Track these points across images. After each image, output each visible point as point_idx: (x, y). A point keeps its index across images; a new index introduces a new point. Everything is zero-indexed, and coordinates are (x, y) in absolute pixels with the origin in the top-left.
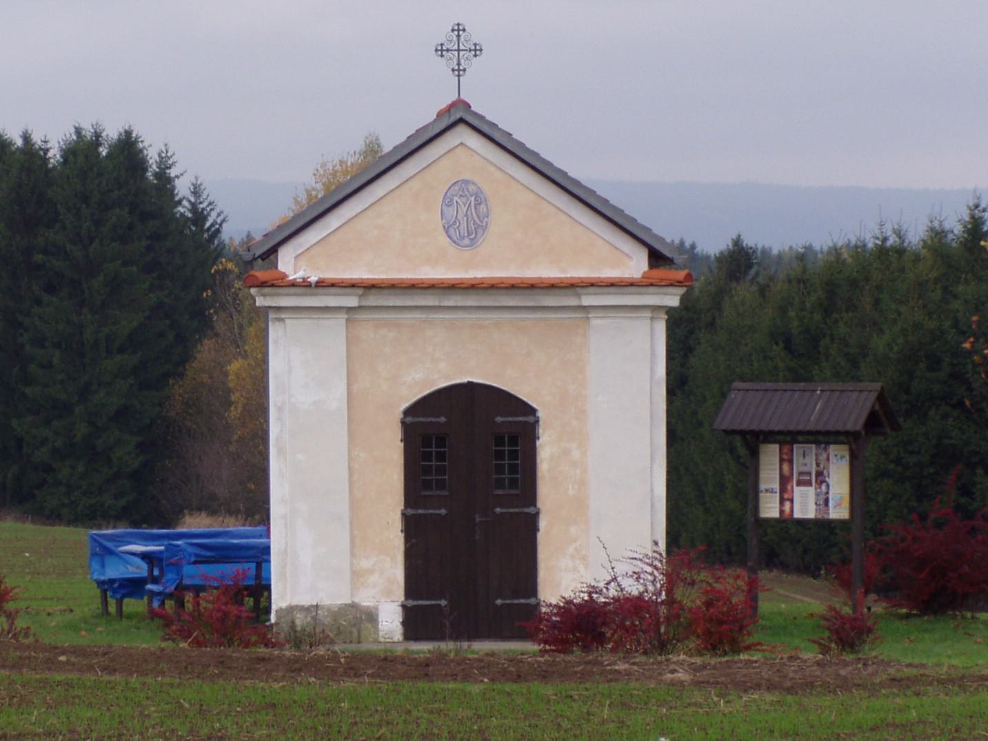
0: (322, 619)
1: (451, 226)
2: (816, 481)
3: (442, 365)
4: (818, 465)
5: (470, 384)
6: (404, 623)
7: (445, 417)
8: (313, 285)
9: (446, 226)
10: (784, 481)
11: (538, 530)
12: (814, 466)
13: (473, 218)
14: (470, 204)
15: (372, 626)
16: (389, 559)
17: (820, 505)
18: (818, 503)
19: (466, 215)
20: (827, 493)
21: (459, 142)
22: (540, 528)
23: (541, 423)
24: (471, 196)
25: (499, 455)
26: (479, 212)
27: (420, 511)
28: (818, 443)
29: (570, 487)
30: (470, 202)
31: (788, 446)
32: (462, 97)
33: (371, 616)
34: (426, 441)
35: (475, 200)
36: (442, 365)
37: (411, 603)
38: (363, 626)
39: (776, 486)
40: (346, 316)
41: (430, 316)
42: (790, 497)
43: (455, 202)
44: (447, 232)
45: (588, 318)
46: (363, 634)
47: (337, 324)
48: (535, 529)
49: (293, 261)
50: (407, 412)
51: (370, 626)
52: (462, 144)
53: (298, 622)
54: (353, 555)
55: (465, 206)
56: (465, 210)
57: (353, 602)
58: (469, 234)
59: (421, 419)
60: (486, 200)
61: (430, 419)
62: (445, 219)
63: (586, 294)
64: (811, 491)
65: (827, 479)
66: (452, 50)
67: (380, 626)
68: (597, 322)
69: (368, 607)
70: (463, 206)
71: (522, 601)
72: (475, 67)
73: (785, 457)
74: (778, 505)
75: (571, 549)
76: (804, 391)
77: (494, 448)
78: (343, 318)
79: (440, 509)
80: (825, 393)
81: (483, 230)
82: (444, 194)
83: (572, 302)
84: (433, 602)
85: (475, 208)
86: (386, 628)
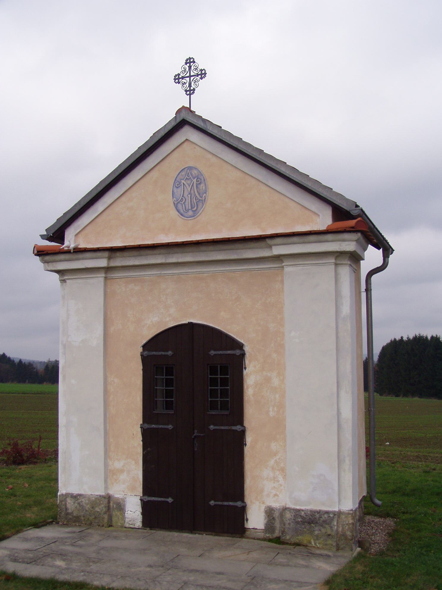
1: (179, 202)
5: (191, 325)
8: (72, 251)
21: (185, 139)
24: (194, 178)
30: (194, 182)
37: (147, 498)
44: (176, 208)
45: (283, 267)
46: (114, 519)
51: (118, 514)
52: (187, 140)
53: (68, 506)
57: (108, 494)
58: (192, 208)
59: (154, 353)
61: (160, 353)
63: (275, 245)
66: (185, 77)
67: (126, 514)
69: (118, 499)
71: (231, 503)
75: (272, 462)
81: (203, 203)
84: (163, 499)
86: (130, 516)
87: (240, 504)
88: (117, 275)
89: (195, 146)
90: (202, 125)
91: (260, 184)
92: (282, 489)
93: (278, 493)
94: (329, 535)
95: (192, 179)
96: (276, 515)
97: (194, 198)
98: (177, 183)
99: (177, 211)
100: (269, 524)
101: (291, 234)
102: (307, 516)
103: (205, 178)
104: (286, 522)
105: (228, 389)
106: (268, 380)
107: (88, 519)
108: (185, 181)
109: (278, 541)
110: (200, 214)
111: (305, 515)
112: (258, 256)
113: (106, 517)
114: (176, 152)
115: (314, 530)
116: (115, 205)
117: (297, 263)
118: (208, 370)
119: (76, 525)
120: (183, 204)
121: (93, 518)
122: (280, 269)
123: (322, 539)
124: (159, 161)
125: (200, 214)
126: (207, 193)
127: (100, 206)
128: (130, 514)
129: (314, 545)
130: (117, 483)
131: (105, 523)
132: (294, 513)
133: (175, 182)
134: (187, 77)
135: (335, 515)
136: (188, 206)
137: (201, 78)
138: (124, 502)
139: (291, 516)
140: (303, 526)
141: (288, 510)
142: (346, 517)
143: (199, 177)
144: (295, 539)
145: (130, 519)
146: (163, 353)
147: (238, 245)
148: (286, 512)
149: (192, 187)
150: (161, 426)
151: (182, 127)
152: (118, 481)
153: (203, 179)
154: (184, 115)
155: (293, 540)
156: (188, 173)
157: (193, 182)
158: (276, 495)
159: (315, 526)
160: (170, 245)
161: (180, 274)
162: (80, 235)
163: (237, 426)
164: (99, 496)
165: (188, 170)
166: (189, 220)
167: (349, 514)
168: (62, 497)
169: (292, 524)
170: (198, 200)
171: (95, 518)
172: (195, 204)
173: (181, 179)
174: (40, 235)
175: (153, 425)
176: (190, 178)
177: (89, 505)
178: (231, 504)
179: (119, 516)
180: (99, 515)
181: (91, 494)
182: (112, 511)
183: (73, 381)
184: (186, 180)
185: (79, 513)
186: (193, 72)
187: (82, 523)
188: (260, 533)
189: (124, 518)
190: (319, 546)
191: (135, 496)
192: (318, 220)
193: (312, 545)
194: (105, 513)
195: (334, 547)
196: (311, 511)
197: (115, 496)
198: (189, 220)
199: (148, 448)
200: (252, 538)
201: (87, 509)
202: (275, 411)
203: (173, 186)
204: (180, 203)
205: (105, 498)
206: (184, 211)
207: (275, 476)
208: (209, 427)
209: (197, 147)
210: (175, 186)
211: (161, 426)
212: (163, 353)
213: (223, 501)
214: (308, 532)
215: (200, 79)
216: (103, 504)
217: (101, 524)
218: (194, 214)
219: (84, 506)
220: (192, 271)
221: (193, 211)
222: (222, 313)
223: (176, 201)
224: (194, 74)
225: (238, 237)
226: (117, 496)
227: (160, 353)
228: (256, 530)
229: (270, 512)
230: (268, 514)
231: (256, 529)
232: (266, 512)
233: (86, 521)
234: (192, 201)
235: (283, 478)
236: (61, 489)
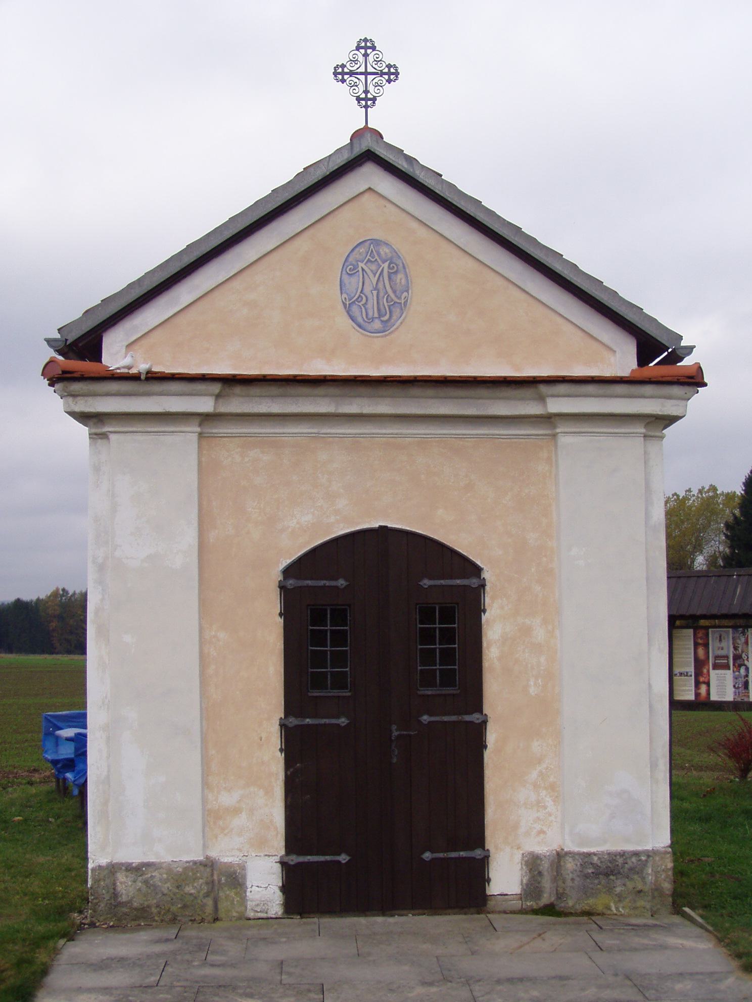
1: (354, 302)
2: (734, 665)
4: (735, 648)
5: (383, 529)
6: (285, 889)
7: (346, 580)
8: (143, 377)
10: (700, 665)
11: (486, 747)
12: (732, 649)
15: (236, 894)
16: (261, 793)
17: (738, 688)
18: (737, 686)
19: (376, 288)
20: (747, 676)
21: (366, 187)
23: (487, 588)
24: (384, 262)
25: (427, 636)
26: (396, 284)
28: (735, 627)
30: (383, 268)
31: (703, 631)
34: (318, 616)
36: (341, 503)
37: (294, 859)
38: (221, 894)
39: (691, 670)
40: (198, 429)
41: (324, 431)
42: (706, 680)
44: (348, 312)
45: (554, 436)
46: (223, 905)
48: (481, 745)
50: (288, 572)
51: (232, 894)
52: (370, 189)
53: (120, 888)
54: (206, 784)
56: (374, 281)
57: (207, 858)
58: (380, 315)
59: (309, 583)
60: (404, 267)
61: (322, 583)
63: (553, 396)
64: (729, 674)
65: (746, 662)
66: (357, 74)
67: (248, 894)
69: (230, 865)
70: (371, 275)
71: (463, 854)
72: (389, 94)
73: (700, 641)
74: (693, 688)
75: (534, 775)
76: (719, 576)
79: (338, 717)
80: (742, 577)
81: (401, 309)
82: (344, 260)
83: (532, 409)
84: (328, 858)
86: (257, 897)
87: (480, 853)
88: (221, 431)
89: (383, 202)
90: (406, 166)
91: (511, 286)
92: (551, 822)
93: (545, 829)
94: (640, 891)
95: (380, 262)
96: (545, 866)
97: (384, 297)
98: (350, 267)
99: (349, 318)
100: (532, 885)
101: (259, 377)
102: (604, 864)
103: (405, 263)
104: (567, 876)
105: (455, 648)
106: (526, 631)
107: (169, 910)
108: (365, 264)
109: (549, 910)
110: (397, 328)
111: (599, 862)
112: (517, 413)
113: (209, 902)
114: (346, 208)
115: (615, 885)
116: (216, 294)
117: (583, 430)
118: (416, 614)
119: (139, 925)
120: (362, 307)
121: (180, 908)
122: (546, 439)
123: (627, 900)
124: (313, 221)
125: (397, 328)
126: (410, 291)
127: (184, 293)
128: (258, 892)
129: (615, 912)
130: (225, 835)
131: (207, 914)
132: (581, 859)
133: (346, 264)
134: (361, 74)
135: (649, 856)
136: (373, 312)
137: (389, 81)
138: (243, 869)
139: (575, 866)
140: (596, 881)
141: (570, 855)
142: (662, 858)
143: (394, 261)
144: (583, 905)
145: (258, 902)
146: (328, 583)
147: (482, 392)
148: (567, 860)
149: (379, 277)
150: (323, 721)
151: (360, 165)
152: (226, 831)
153: (401, 265)
154: (367, 143)
155: (579, 908)
156: (372, 251)
157: (381, 269)
158: (542, 832)
159: (616, 879)
160: (358, 381)
161: (357, 436)
162: (136, 347)
163: (474, 715)
164: (191, 864)
165: (372, 245)
166: (374, 337)
167: (666, 853)
168: (98, 871)
169: (578, 879)
170: (392, 303)
171: (185, 907)
172: (386, 309)
173: (358, 261)
174: (695, 347)
175: (308, 720)
176: (376, 260)
177: (169, 883)
178: (462, 855)
179: (234, 898)
180: (193, 901)
181: (172, 861)
182: (218, 890)
183: (128, 638)
184: (367, 262)
185: (147, 900)
186: (372, 66)
187: (154, 920)
188: (515, 902)
189: (243, 900)
190: (623, 911)
191: (267, 857)
192: (612, 359)
193: (612, 911)
194: (207, 895)
195: (647, 910)
196: (609, 854)
197: (222, 860)
198: (374, 337)
199: (297, 764)
200: (500, 912)
201: (166, 892)
202: (539, 686)
203: (342, 272)
204: (356, 304)
205: (205, 866)
206: (364, 320)
207: (540, 799)
208: (419, 719)
209: (389, 205)
210: (346, 271)
211: (323, 721)
212: (328, 583)
213: (446, 851)
214: (604, 890)
215: (387, 83)
216: (202, 879)
217: (198, 918)
218: (384, 327)
219: (159, 885)
220: (384, 431)
221: (382, 321)
222: (440, 512)
223: (347, 300)
224: (375, 71)
225: (219, 374)
226: (226, 861)
227: (322, 583)
228: (506, 897)
229: (533, 863)
230: (531, 867)
231: (507, 895)
232: (527, 863)
233: (163, 915)
234: (381, 303)
235: (554, 801)
236: (94, 857)
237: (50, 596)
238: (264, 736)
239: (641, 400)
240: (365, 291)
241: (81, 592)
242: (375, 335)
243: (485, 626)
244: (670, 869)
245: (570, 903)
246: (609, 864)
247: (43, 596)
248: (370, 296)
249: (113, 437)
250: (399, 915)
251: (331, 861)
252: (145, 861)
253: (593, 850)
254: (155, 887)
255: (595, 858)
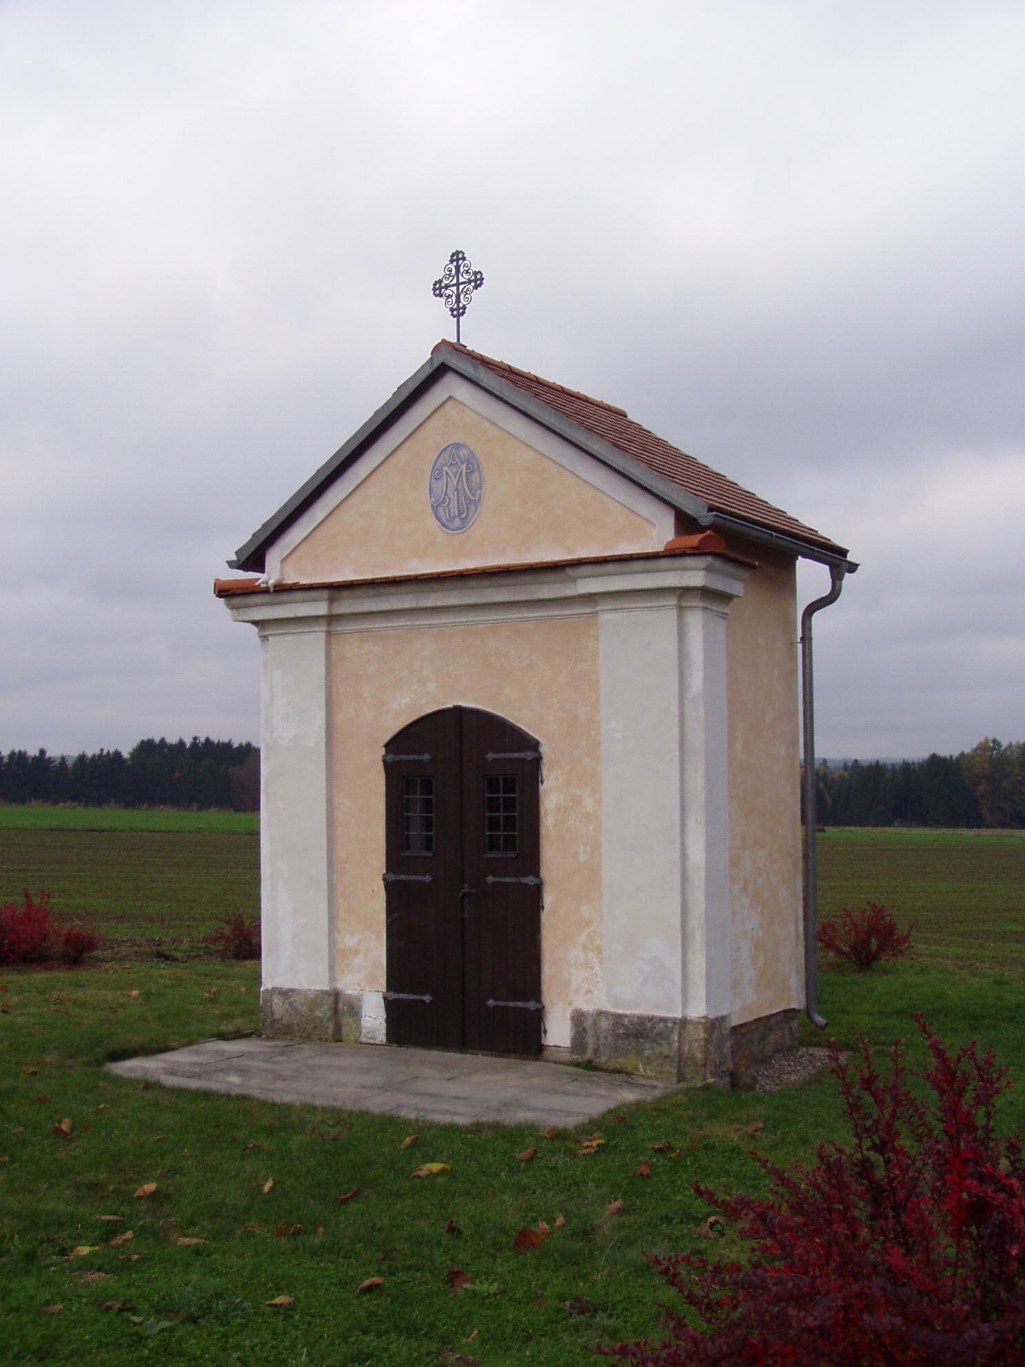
0: (299, 1007)
1: (439, 504)
3: (431, 686)
8: (271, 590)
9: (435, 505)
11: (543, 908)
13: (465, 492)
14: (461, 473)
21: (447, 396)
22: (545, 906)
24: (462, 464)
25: (493, 805)
27: (402, 877)
29: (581, 850)
32: (461, 342)
33: (354, 1010)
35: (467, 468)
36: (431, 686)
43: (444, 473)
44: (435, 514)
45: (597, 613)
46: (345, 1030)
47: (315, 639)
49: (279, 564)
50: (395, 744)
55: (456, 477)
56: (455, 482)
58: (460, 514)
60: (478, 466)
62: (434, 496)
66: (450, 286)
67: (362, 1022)
68: (609, 618)
70: (453, 477)
71: (519, 1004)
72: (477, 301)
77: (487, 795)
78: (322, 631)
79: (424, 875)
81: (476, 505)
85: (467, 479)
86: (369, 1025)
88: (344, 628)
94: (666, 1057)
96: (588, 1023)
100: (577, 1039)
106: (577, 801)
109: (590, 1066)
113: (331, 1025)
114: (433, 418)
127: (318, 512)
142: (695, 1028)
153: (476, 466)
158: (589, 991)
167: (699, 1023)
169: (610, 1038)
171: (315, 1027)
190: (650, 1074)
194: (329, 1020)
196: (639, 1017)
200: (551, 1062)
201: (303, 1013)
217: (324, 1037)
220: (461, 620)
222: (507, 691)
228: (559, 1049)
229: (578, 1019)
231: (559, 1047)
234: (460, 502)
237: (977, 749)
238: (375, 888)
239: (659, 574)
240: (448, 493)
241: (1018, 744)
242: (457, 532)
243: (543, 796)
244: (702, 1040)
245: (603, 1060)
246: (638, 1027)
247: (967, 750)
248: (451, 497)
249: (270, 638)
250: (471, 1053)
251: (419, 1000)
252: (292, 987)
253: (627, 1012)
254: (296, 1008)
255: (626, 1020)
